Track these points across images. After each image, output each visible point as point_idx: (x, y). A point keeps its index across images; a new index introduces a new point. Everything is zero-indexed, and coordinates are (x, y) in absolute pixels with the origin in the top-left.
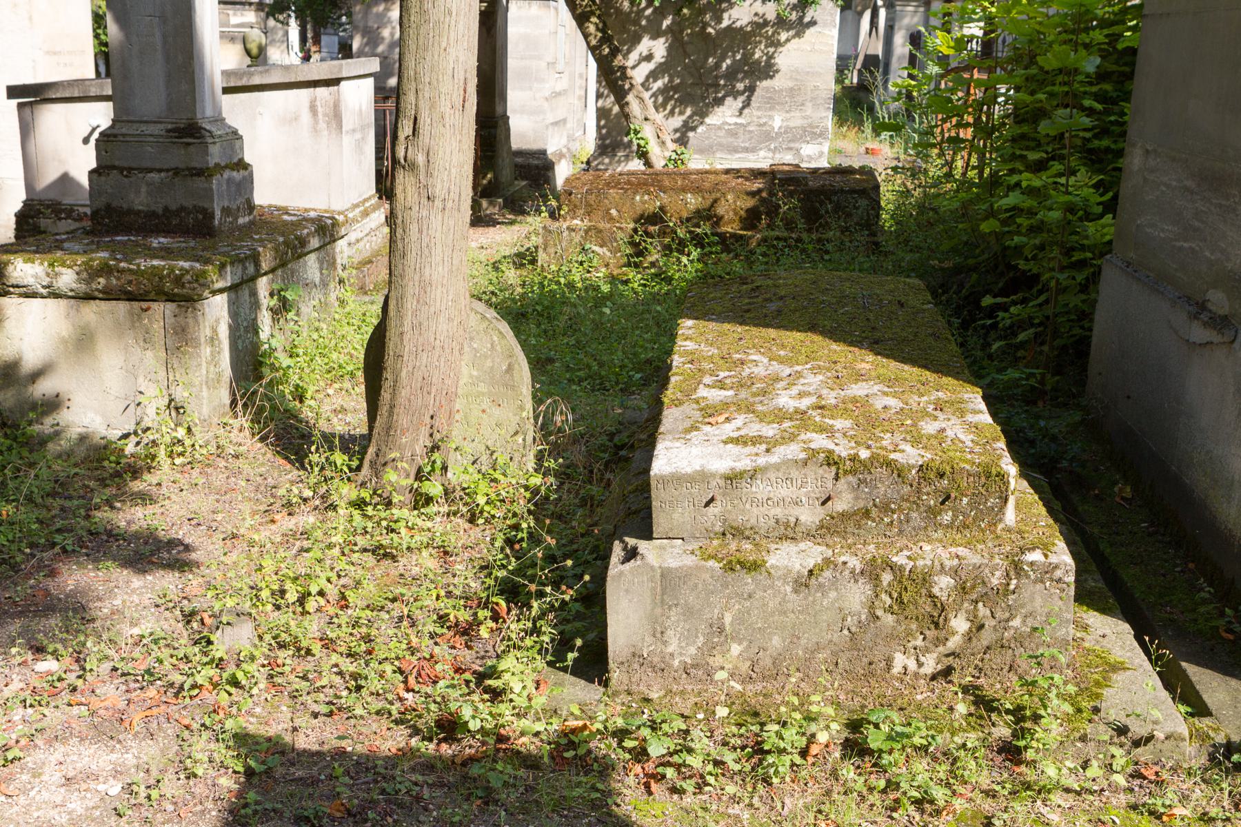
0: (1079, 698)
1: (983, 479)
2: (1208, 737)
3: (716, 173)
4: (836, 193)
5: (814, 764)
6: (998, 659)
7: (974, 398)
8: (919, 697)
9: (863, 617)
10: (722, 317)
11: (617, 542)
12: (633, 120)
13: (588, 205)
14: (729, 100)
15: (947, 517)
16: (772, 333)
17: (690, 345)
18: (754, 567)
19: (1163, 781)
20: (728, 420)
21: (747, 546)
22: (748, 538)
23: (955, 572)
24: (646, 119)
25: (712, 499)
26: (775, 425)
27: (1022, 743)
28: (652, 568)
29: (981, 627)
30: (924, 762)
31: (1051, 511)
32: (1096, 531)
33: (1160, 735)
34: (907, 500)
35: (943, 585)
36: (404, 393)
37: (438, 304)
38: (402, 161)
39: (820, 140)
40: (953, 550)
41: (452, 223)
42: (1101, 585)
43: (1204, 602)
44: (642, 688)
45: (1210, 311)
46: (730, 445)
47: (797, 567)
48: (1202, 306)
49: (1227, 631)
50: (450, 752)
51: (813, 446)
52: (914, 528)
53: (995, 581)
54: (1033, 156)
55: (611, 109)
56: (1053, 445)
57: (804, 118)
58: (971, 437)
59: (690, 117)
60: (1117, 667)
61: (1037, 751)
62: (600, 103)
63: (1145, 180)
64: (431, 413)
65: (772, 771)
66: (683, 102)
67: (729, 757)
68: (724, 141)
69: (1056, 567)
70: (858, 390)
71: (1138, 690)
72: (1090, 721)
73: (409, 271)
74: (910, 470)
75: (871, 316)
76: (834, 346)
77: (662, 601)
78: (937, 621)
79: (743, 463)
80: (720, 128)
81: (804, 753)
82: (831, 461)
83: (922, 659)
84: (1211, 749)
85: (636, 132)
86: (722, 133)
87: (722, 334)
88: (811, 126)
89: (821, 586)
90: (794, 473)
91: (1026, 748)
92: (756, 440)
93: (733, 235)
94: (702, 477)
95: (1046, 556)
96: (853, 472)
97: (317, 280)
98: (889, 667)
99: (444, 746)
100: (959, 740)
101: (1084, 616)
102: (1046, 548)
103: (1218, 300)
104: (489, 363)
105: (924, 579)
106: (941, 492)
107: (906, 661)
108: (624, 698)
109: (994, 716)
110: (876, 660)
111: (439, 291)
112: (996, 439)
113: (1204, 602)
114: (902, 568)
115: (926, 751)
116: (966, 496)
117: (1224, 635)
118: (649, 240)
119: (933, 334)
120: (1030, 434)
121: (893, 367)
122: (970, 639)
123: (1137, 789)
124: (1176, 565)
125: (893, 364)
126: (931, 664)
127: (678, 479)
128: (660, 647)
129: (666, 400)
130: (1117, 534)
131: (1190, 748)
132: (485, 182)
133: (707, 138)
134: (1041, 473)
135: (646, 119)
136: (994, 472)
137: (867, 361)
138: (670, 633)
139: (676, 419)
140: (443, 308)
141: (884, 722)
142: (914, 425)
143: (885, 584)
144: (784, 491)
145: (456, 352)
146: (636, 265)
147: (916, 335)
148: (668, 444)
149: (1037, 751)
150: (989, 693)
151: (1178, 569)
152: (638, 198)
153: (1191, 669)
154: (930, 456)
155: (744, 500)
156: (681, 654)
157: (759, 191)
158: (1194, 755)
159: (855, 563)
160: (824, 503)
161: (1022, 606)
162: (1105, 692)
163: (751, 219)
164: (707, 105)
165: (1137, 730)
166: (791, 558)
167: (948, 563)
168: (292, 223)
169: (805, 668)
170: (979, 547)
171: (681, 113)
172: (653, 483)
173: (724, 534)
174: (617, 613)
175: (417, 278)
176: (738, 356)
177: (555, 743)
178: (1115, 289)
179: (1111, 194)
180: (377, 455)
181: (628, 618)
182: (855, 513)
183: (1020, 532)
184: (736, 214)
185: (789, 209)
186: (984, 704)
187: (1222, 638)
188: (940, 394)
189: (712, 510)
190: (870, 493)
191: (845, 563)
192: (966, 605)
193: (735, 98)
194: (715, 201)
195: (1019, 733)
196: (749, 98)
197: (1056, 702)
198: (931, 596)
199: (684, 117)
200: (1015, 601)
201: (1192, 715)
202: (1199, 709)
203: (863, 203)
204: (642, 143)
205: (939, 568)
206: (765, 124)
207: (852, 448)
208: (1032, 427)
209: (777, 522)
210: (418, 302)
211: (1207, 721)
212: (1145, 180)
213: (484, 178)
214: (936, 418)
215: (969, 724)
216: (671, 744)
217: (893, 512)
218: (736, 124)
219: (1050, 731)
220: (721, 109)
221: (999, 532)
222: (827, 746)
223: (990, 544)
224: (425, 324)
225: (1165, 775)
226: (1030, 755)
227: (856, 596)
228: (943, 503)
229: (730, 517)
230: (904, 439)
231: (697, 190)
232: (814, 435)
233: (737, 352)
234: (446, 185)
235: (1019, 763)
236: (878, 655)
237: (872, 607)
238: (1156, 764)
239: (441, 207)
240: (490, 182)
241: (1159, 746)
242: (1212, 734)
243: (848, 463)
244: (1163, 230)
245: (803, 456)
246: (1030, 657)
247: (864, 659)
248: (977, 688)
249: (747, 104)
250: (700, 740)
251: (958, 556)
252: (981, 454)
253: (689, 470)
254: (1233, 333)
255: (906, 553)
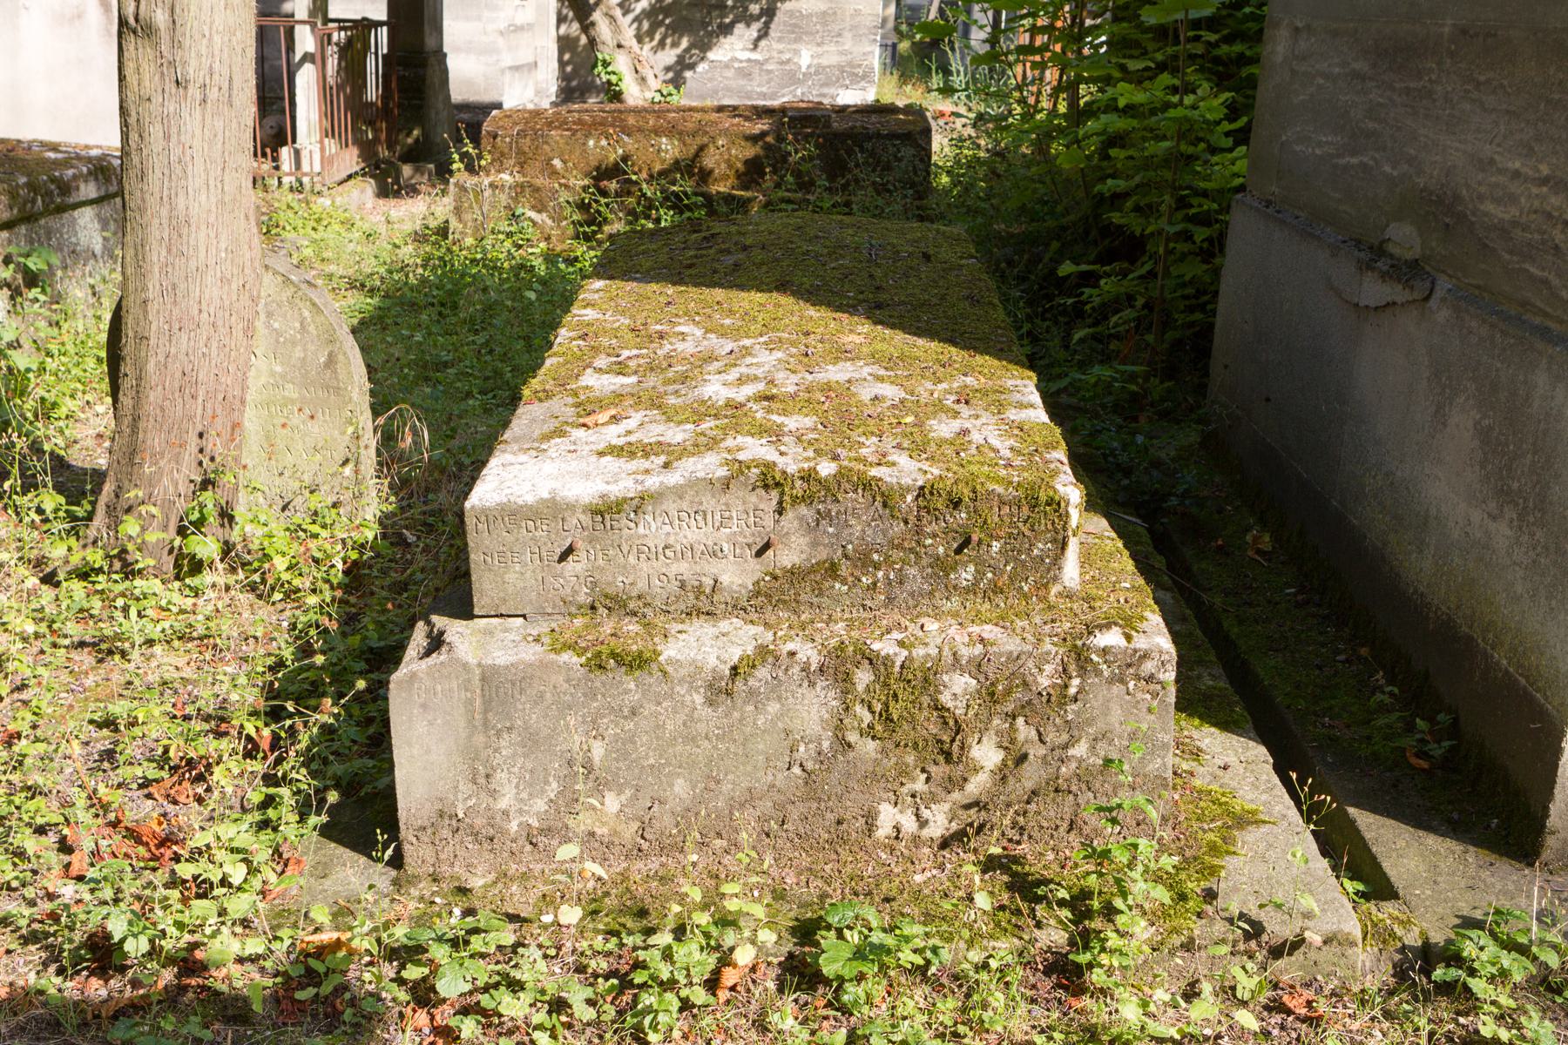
0: (1183, 876)
1: (1025, 511)
2: (1393, 935)
3: (703, 110)
4: (870, 138)
5: (728, 1002)
6: (1049, 811)
7: (1025, 389)
8: (918, 878)
9: (826, 744)
10: (648, 276)
11: (421, 624)
12: (600, 47)
13: (520, 152)
14: (740, 28)
15: (966, 575)
16: (719, 294)
17: (590, 314)
18: (637, 663)
19: (1320, 1018)
20: (615, 419)
21: (632, 627)
22: (635, 614)
23: (977, 667)
24: (619, 46)
25: (570, 550)
26: (690, 426)
27: (1083, 958)
28: (465, 665)
29: (1023, 758)
30: (919, 993)
31: (1144, 567)
32: (1218, 600)
33: (1314, 938)
34: (899, 547)
35: (958, 688)
36: (153, 397)
37: (202, 254)
38: (132, 21)
39: (863, 84)
40: (975, 629)
41: (219, 124)
42: (1223, 684)
43: (1383, 709)
44: (458, 869)
45: (1391, 256)
46: (609, 458)
47: (712, 661)
48: (1379, 251)
49: (1417, 756)
50: (103, 993)
51: (741, 456)
52: (912, 594)
53: (1044, 682)
54: (1134, 65)
55: (578, 39)
56: (1155, 473)
57: (841, 53)
58: (1012, 442)
59: (687, 50)
60: (1245, 820)
61: (1110, 972)
62: (563, 30)
63: (1294, 73)
64: (199, 428)
65: (647, 1021)
66: (677, 29)
67: (577, 996)
68: (733, 84)
69: (1146, 656)
70: (836, 373)
71: (1277, 859)
72: (1199, 915)
73: (151, 201)
74: (903, 496)
75: (878, 273)
76: (812, 312)
77: (486, 723)
78: (949, 750)
79: (622, 484)
80: (727, 66)
81: (712, 984)
82: (770, 480)
83: (926, 813)
84: (1397, 957)
85: (606, 64)
86: (730, 73)
87: (642, 298)
88: (850, 64)
89: (752, 693)
90: (709, 503)
91: (1090, 966)
92: (647, 451)
93: (728, 199)
94: (553, 510)
95: (1128, 638)
96: (807, 499)
97: (98, 248)
98: (870, 827)
99: (95, 983)
100: (976, 956)
101: (1196, 734)
102: (1129, 625)
103: (1404, 238)
104: (298, 353)
105: (926, 680)
106: (958, 532)
107: (899, 817)
108: (426, 888)
109: (1040, 910)
110: (848, 816)
111: (202, 235)
112: (1050, 446)
113: (1383, 709)
114: (887, 661)
115: (924, 974)
116: (998, 538)
117: (1414, 761)
118: (603, 201)
119: (970, 297)
120: (1123, 458)
121: (897, 341)
122: (1004, 778)
123: (1275, 1032)
124: (1337, 652)
125: (899, 337)
126: (939, 822)
127: (512, 514)
128: (485, 800)
129: (526, 392)
130: (1250, 605)
131: (1363, 956)
132: (410, 141)
133: (710, 80)
134: (1139, 516)
135: (619, 46)
136: (1043, 497)
137: (859, 332)
138: (501, 776)
139: (534, 420)
140: (211, 262)
141: (850, 928)
142: (919, 424)
143: (860, 688)
144: (692, 533)
145: (238, 332)
146: (588, 238)
147: (943, 298)
148: (508, 457)
149: (1110, 972)
150: (1035, 868)
151: (1342, 657)
152: (591, 143)
153: (1364, 820)
154: (936, 472)
155: (625, 548)
156: (520, 811)
157: (763, 134)
158: (1369, 967)
159: (808, 653)
160: (759, 553)
161: (1090, 722)
162: (1230, 862)
163: (751, 173)
164: (710, 34)
165: (1277, 929)
166: (702, 647)
167: (965, 652)
168: (55, 162)
169: (722, 830)
170: (1019, 623)
171: (675, 45)
172: (470, 521)
173: (593, 608)
174: (410, 745)
175: (164, 212)
176: (658, 327)
177: (285, 974)
178: (1246, 233)
179: (1245, 119)
180: (117, 496)
181: (428, 751)
182: (812, 570)
183: (1088, 599)
184: (730, 167)
185: (803, 158)
186: (1026, 889)
187: (1412, 767)
188: (969, 380)
189: (570, 566)
190: (837, 535)
191: (792, 654)
192: (996, 721)
193: (748, 26)
194: (702, 148)
195: (1083, 939)
196: (767, 25)
197: (1141, 885)
198: (938, 707)
199: (678, 51)
200: (1077, 713)
201: (1364, 895)
202: (1378, 888)
203: (907, 152)
204: (614, 79)
205: (950, 660)
206: (789, 61)
207: (808, 459)
208: (1125, 447)
209: (683, 586)
210: (169, 251)
211: (1390, 908)
212: (1294, 73)
213: (408, 135)
214: (956, 415)
215: (998, 925)
216: (483, 972)
217: (877, 567)
218: (749, 60)
219: (1134, 933)
220: (730, 39)
221: (1052, 598)
222: (753, 969)
223: (1037, 620)
224: (182, 286)
225: (1322, 1007)
226: (1097, 977)
227: (813, 709)
228: (959, 551)
229: (604, 578)
230: (899, 446)
231: (672, 131)
232: (749, 439)
233: (659, 322)
234: (206, 63)
235: (1079, 991)
236: (851, 808)
237: (839, 728)
238: (1308, 985)
239: (198, 97)
240: (417, 141)
241: (1312, 955)
242: (1399, 931)
243: (798, 483)
244: (1320, 144)
245: (722, 472)
246: (1100, 809)
247: (829, 815)
248: (1015, 860)
249: (764, 34)
250: (533, 968)
251: (982, 640)
252: (1024, 469)
253: (530, 499)
254: (1428, 284)
255: (896, 635)
